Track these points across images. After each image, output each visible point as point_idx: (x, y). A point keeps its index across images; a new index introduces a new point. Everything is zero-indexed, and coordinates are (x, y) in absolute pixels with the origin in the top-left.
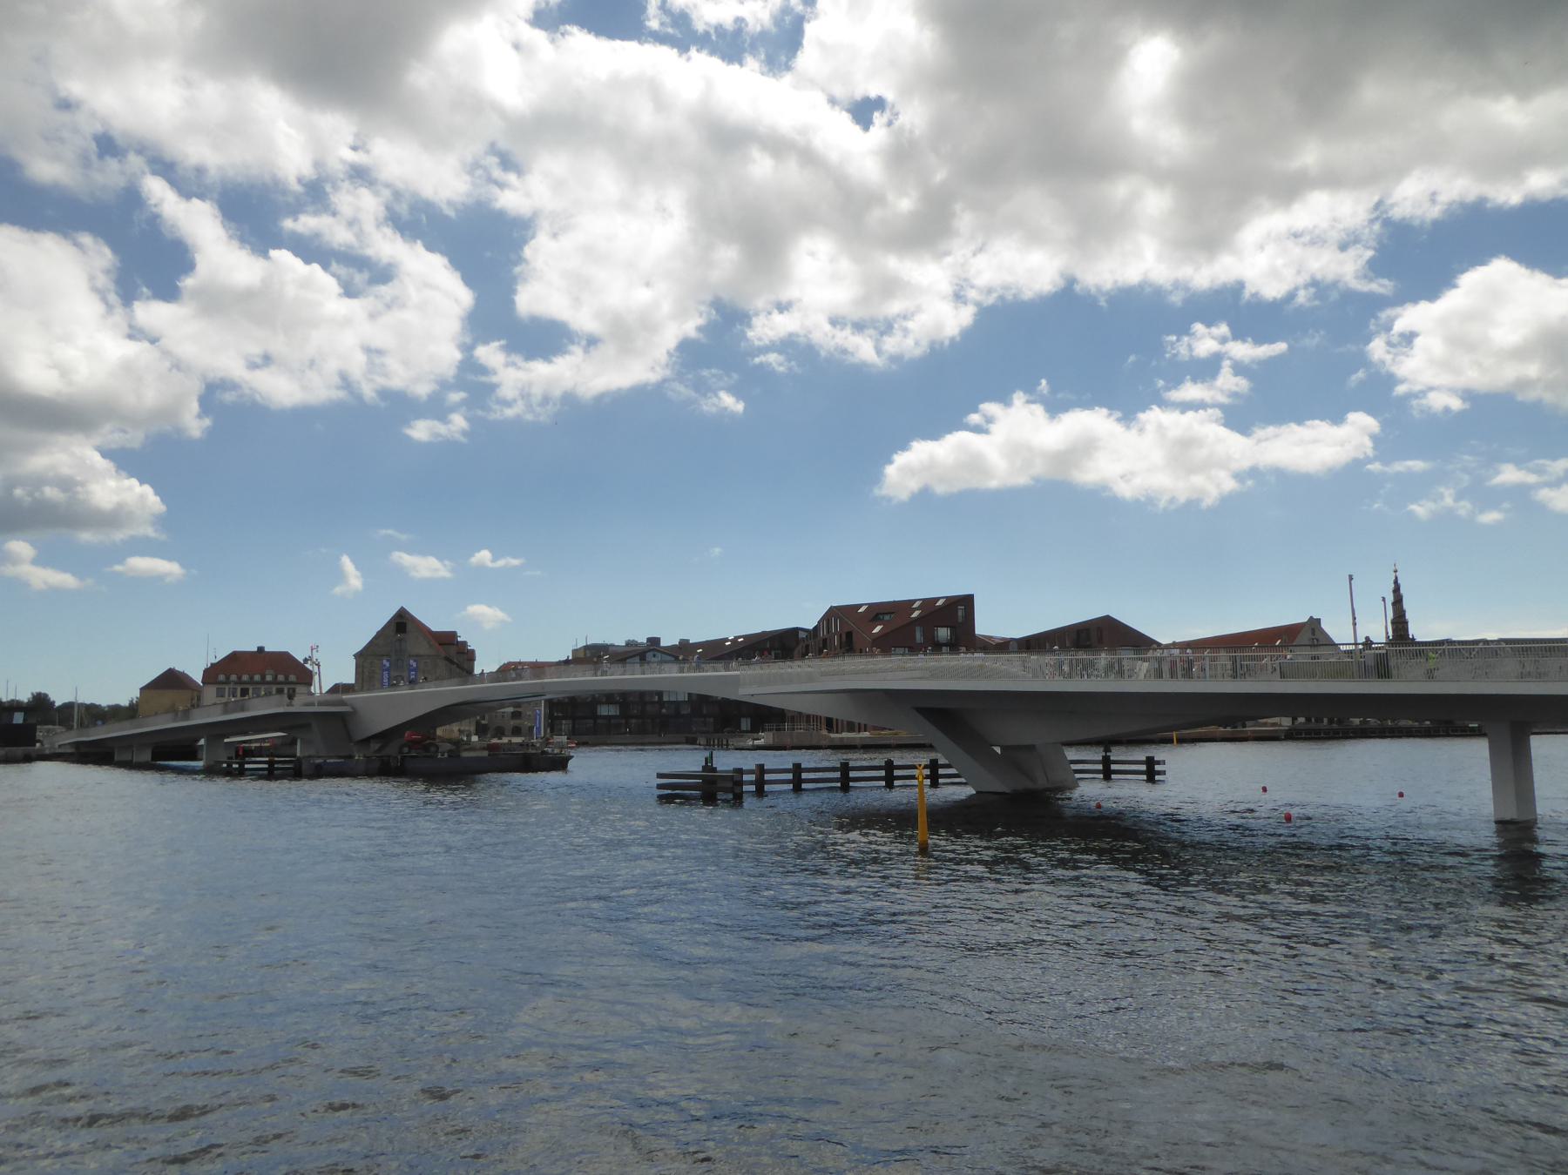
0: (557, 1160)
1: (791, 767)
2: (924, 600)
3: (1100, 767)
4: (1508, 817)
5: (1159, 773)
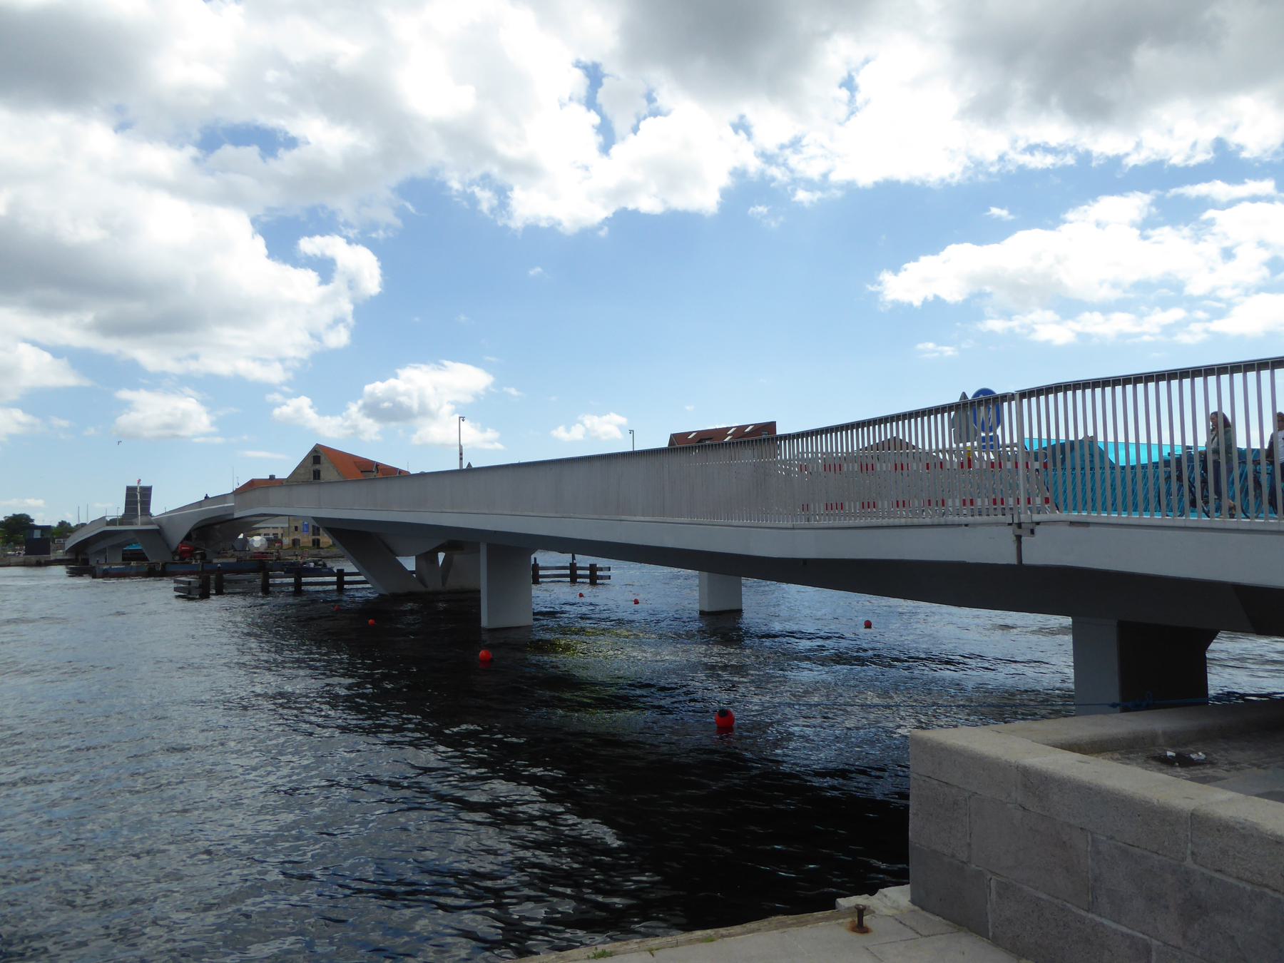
1: (589, 566)
2: (755, 425)
3: (568, 572)
4: (706, 609)
5: (602, 577)
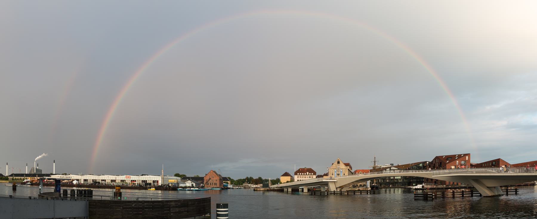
0: (502, 205)
3: (509, 193)
5: (518, 192)
